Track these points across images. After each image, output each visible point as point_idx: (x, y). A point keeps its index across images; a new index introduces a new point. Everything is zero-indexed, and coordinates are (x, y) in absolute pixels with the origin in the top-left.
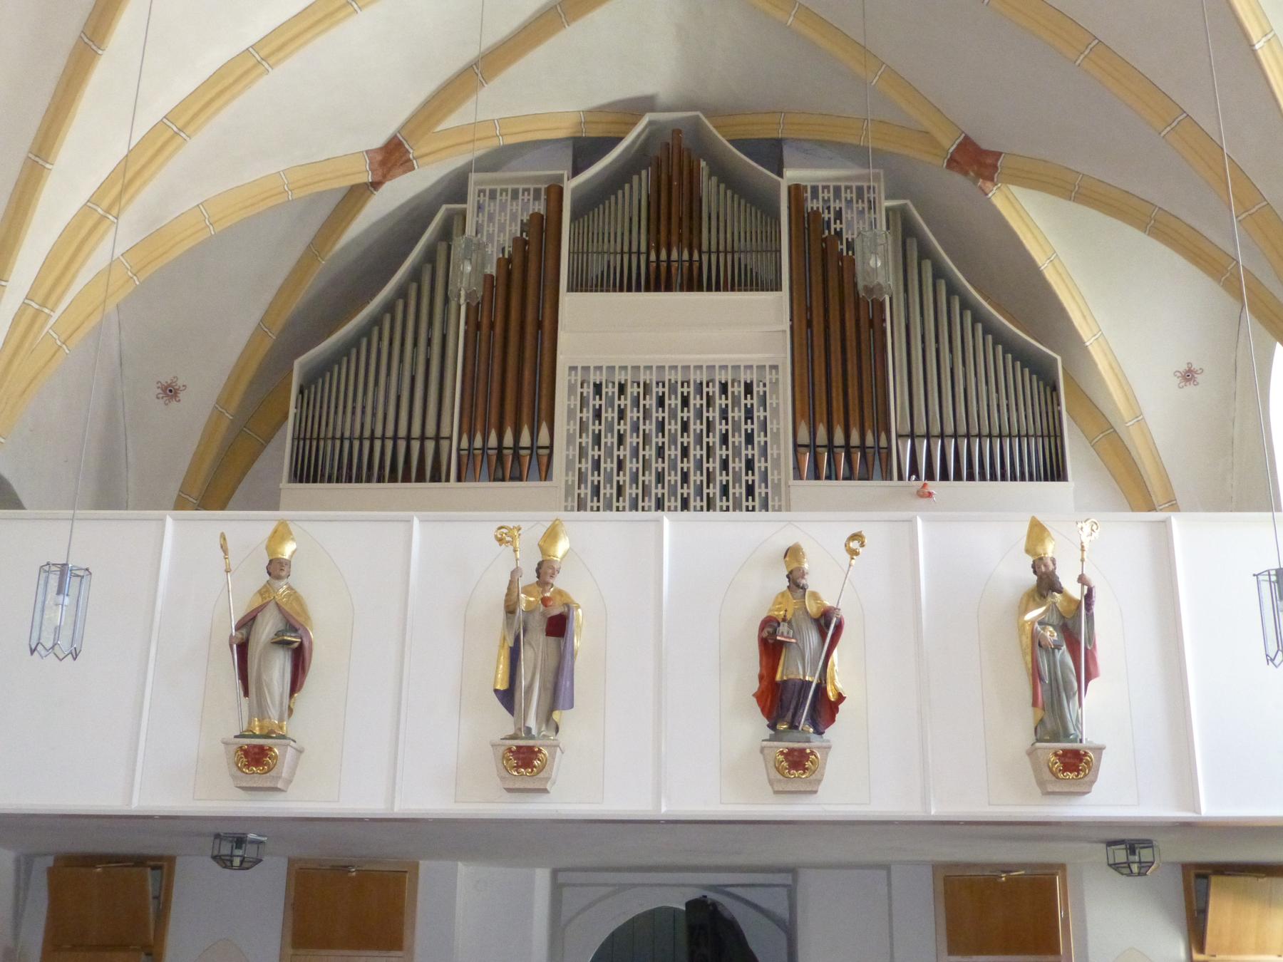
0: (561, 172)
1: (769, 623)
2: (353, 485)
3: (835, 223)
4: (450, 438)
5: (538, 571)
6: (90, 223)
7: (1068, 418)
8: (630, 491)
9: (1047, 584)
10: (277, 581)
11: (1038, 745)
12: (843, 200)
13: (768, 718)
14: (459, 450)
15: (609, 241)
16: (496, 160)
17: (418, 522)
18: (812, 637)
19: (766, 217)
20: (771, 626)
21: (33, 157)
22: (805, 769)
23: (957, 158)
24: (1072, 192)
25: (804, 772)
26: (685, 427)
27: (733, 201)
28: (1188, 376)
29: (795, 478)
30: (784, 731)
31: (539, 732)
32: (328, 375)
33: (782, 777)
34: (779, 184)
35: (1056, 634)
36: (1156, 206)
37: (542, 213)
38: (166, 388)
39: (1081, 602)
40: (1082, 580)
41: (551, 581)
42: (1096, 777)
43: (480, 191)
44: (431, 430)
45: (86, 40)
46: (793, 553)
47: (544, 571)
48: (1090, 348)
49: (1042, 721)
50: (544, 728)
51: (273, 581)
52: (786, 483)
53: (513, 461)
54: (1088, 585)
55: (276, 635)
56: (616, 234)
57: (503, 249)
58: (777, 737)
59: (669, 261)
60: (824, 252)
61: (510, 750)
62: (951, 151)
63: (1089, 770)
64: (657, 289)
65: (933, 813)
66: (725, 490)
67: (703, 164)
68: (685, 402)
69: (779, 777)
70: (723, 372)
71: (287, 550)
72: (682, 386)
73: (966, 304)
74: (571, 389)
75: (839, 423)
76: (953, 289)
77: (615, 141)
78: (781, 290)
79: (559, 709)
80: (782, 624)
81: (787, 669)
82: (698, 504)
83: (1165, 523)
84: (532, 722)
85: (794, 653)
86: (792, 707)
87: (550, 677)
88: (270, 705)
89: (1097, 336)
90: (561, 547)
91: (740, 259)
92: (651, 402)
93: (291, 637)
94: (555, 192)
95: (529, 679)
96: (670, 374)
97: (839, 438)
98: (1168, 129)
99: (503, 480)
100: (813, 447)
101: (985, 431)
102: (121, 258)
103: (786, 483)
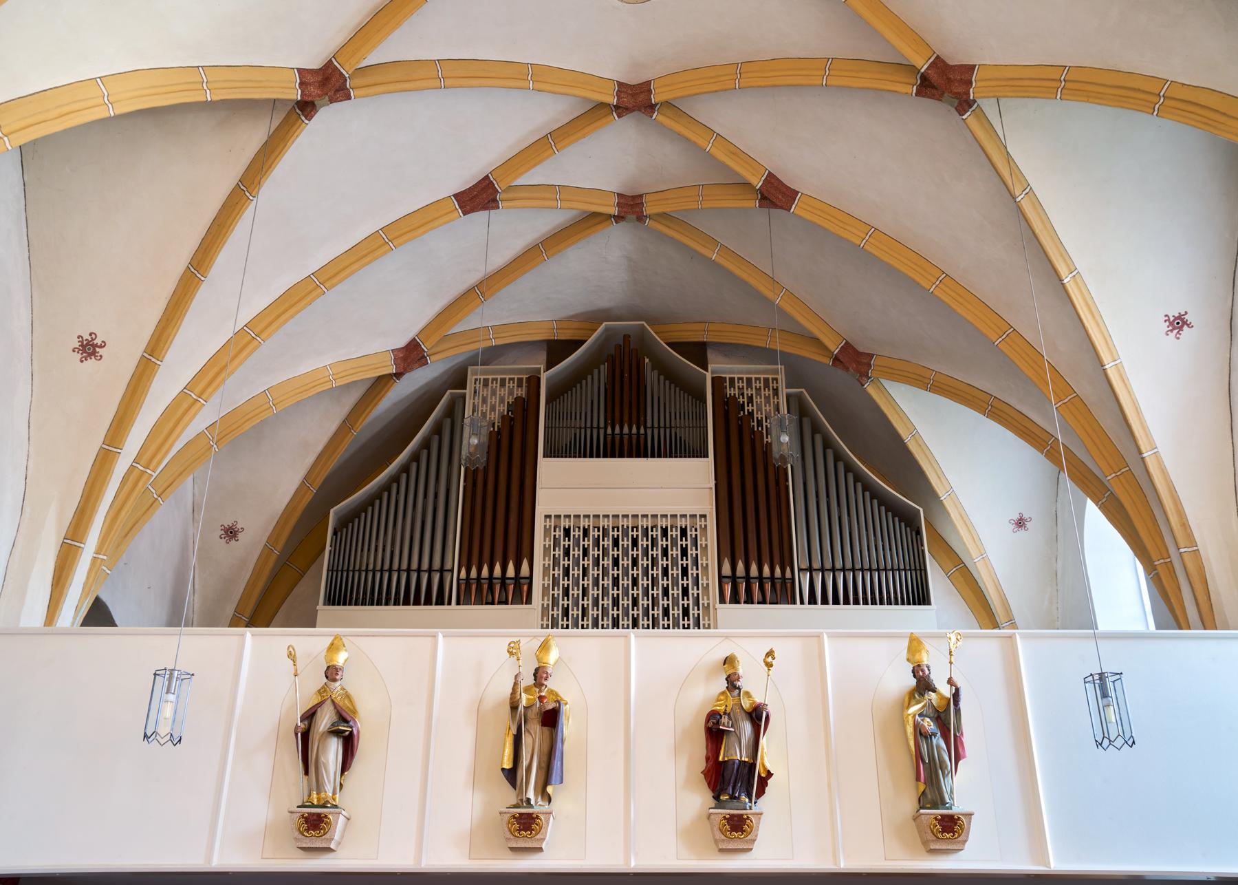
0: (539, 366)
1: (713, 717)
2: (375, 607)
3: (748, 406)
4: (452, 570)
5: (535, 675)
6: (185, 405)
7: (930, 558)
8: (592, 612)
9: (923, 685)
10: (332, 683)
11: (922, 811)
12: (771, 388)
13: (713, 791)
14: (458, 579)
15: (576, 419)
16: (491, 355)
17: (250, 636)
18: (747, 729)
19: (696, 401)
20: (715, 718)
21: (147, 356)
22: (743, 831)
23: (841, 357)
24: (928, 384)
25: (742, 834)
26: (635, 562)
27: (670, 389)
28: (1020, 523)
29: (720, 603)
30: (726, 801)
31: (536, 802)
32: (357, 520)
33: (725, 838)
34: (705, 375)
35: (932, 724)
36: (992, 396)
37: (524, 396)
38: (228, 530)
39: (950, 699)
40: (950, 682)
41: (545, 683)
42: (968, 837)
43: (476, 380)
44: (437, 564)
45: (193, 270)
46: (729, 661)
47: (540, 675)
48: (944, 501)
49: (924, 792)
50: (539, 799)
51: (329, 683)
52: (714, 606)
53: (488, 591)
54: (956, 686)
55: (332, 725)
56: (581, 413)
57: (494, 424)
58: (719, 804)
59: (621, 434)
60: (740, 428)
61: (514, 817)
62: (835, 353)
63: (962, 832)
64: (613, 456)
65: (842, 867)
66: (666, 612)
67: (647, 360)
68: (635, 542)
69: (723, 837)
70: (664, 519)
71: (341, 658)
72: (633, 531)
73: (849, 468)
74: (547, 531)
75: (754, 560)
76: (839, 457)
77: (579, 343)
78: (708, 457)
79: (551, 785)
80: (723, 716)
81: (728, 751)
82: (646, 623)
83: (1011, 637)
84: (531, 794)
85: (733, 739)
86: (732, 781)
87: (545, 758)
88: (326, 781)
89: (949, 493)
90: (552, 657)
91: (676, 433)
92: (608, 543)
93: (344, 726)
94: (534, 381)
95: (528, 760)
96: (623, 521)
97: (754, 571)
98: (1000, 339)
99: (493, 603)
100: (734, 578)
101: (867, 566)
102: (205, 431)
103: (714, 606)
